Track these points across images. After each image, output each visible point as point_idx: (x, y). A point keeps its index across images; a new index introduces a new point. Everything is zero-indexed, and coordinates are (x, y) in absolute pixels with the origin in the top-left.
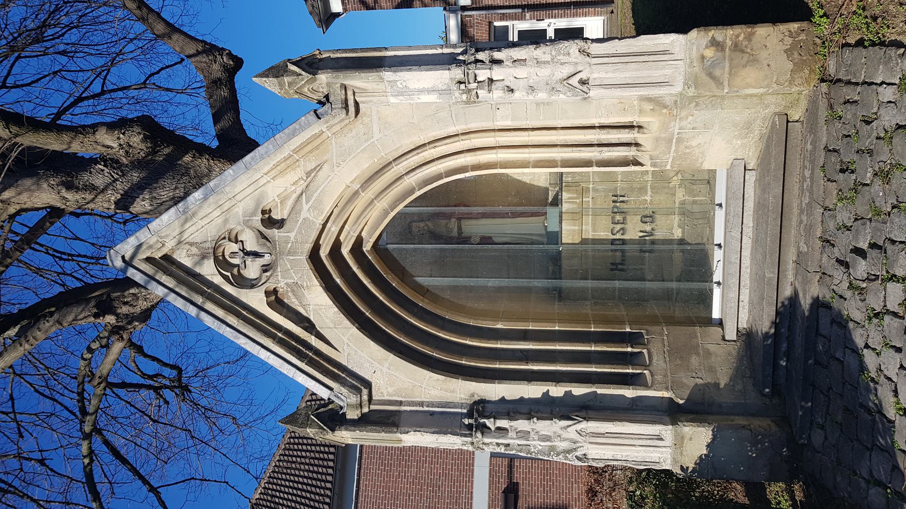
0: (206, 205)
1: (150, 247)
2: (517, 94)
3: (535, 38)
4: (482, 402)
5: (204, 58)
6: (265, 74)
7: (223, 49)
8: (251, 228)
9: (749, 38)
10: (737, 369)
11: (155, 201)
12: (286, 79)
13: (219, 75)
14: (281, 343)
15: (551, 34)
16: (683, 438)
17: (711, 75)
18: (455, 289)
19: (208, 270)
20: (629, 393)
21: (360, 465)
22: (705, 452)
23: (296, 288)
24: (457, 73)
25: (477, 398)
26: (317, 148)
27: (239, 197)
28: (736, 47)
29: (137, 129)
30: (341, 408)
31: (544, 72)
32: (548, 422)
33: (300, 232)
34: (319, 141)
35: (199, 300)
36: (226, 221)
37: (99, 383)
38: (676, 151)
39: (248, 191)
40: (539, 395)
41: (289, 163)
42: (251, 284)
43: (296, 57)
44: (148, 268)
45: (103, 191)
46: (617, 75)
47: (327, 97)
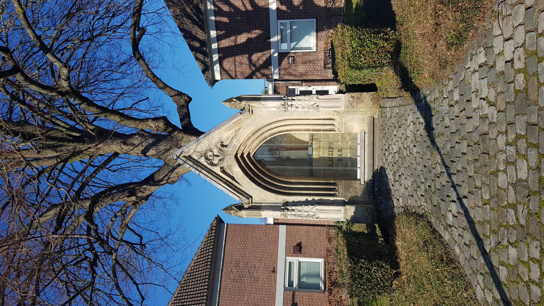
0: (204, 139)
1: (185, 152)
2: (299, 109)
3: (303, 93)
4: (287, 202)
5: (178, 97)
6: (225, 101)
7: (185, 94)
8: (216, 147)
9: (361, 95)
10: (363, 192)
11: (157, 150)
12: (232, 103)
13: (183, 104)
14: (225, 183)
15: (314, 92)
16: (347, 210)
17: (351, 105)
18: (279, 169)
19: (203, 161)
20: (332, 199)
21: (219, 295)
22: (353, 214)
23: (230, 166)
24: (282, 102)
25: (285, 201)
26: (239, 123)
27: (214, 137)
28: (358, 98)
29: (162, 121)
30: (243, 204)
31: (307, 103)
32: (307, 207)
33: (232, 148)
34: (240, 121)
35: (200, 169)
36: (209, 145)
37: (124, 227)
38: (345, 127)
39: (218, 136)
40: (305, 200)
41: (231, 128)
42: (216, 165)
43: (235, 96)
44: (184, 159)
45: (137, 146)
46: (327, 104)
47: (244, 108)
